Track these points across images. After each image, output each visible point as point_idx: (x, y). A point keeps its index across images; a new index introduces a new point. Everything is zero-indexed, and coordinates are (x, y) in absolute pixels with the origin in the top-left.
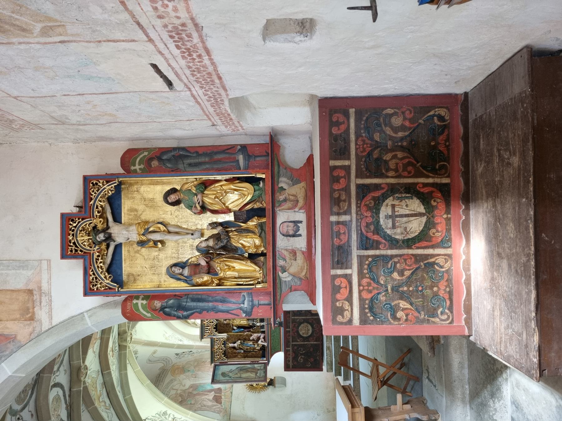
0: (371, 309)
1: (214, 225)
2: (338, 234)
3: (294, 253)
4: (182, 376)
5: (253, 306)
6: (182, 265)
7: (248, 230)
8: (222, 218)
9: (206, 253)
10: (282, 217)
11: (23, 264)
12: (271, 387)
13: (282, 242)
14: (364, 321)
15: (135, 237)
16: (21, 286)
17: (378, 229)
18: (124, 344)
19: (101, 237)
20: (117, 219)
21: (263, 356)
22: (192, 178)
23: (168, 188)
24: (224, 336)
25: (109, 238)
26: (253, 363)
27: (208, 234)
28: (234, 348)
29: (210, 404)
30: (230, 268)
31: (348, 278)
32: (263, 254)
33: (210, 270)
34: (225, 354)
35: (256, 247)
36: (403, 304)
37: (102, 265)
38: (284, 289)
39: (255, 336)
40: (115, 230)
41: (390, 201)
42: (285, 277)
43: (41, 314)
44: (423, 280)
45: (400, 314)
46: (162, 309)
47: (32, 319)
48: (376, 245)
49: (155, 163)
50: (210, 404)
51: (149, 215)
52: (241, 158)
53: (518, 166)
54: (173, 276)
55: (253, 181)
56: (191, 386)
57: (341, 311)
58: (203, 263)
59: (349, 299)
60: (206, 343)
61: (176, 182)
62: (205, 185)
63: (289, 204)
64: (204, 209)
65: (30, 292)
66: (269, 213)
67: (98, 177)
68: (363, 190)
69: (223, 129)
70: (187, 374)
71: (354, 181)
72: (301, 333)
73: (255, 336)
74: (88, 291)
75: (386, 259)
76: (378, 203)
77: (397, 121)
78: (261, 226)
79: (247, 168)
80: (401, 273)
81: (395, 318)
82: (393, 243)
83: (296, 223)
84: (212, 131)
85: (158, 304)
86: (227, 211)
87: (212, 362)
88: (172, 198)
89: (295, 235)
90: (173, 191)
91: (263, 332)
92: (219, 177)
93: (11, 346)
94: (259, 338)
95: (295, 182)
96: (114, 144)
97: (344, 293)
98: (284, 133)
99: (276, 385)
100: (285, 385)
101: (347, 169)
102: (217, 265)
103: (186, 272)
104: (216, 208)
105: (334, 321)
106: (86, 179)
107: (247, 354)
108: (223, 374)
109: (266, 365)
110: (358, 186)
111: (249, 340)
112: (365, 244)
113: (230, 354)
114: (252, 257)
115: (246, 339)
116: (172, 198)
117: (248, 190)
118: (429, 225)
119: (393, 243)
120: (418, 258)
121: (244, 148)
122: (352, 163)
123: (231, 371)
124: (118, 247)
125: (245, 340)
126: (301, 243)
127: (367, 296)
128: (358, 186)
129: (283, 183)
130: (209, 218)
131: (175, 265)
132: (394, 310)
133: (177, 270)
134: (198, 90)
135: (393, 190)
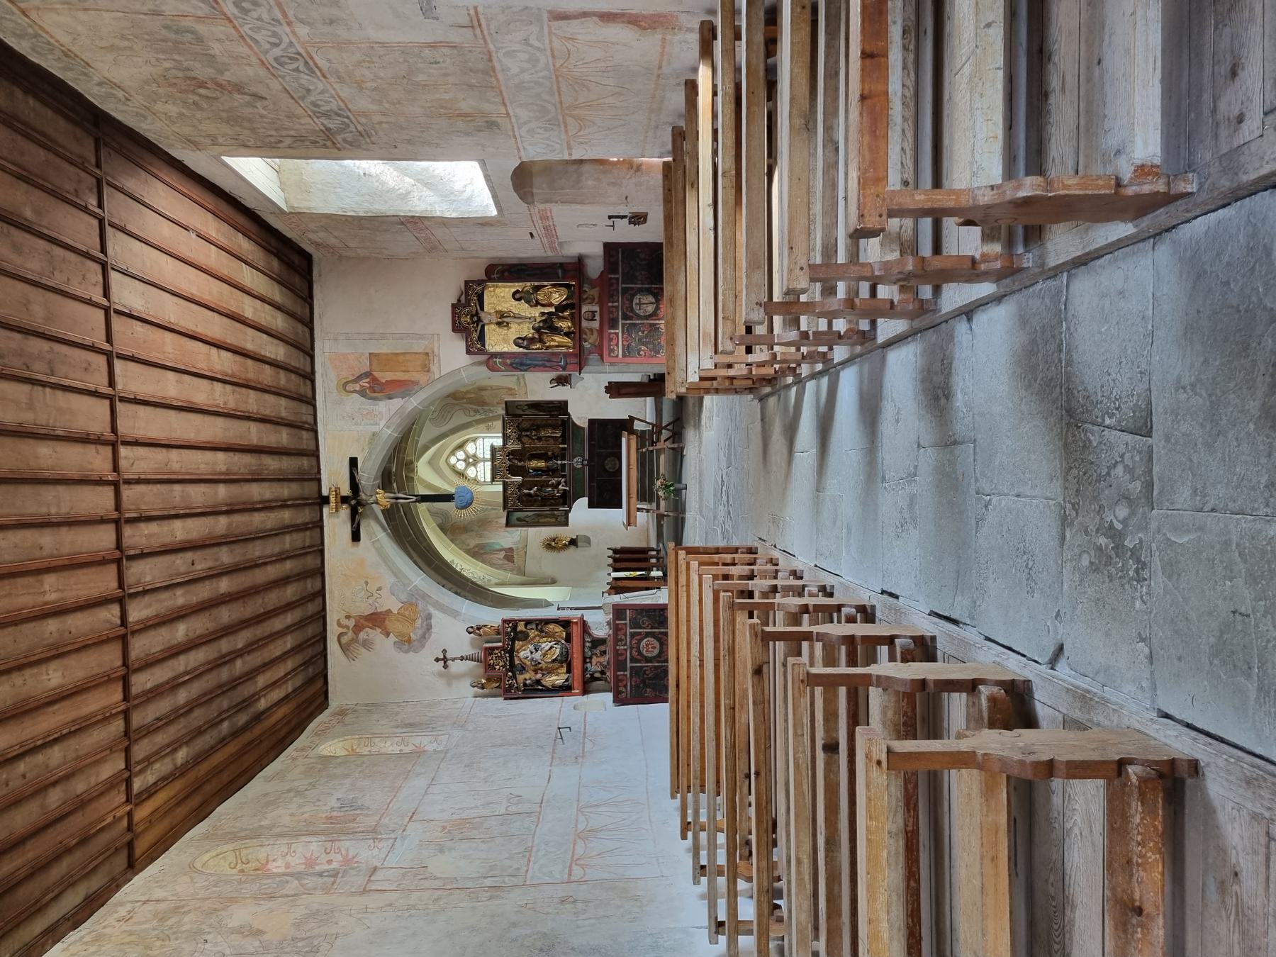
0: (628, 349)
1: (543, 314)
2: (612, 312)
3: (591, 330)
4: (464, 536)
5: (566, 364)
6: (523, 339)
7: (564, 318)
8: (547, 310)
9: (537, 330)
10: (585, 309)
11: (422, 337)
12: (572, 548)
13: (585, 324)
14: (624, 356)
15: (494, 320)
16: (421, 350)
17: (632, 310)
18: (411, 475)
19: (475, 319)
20: (482, 309)
21: (564, 504)
22: (529, 284)
23: (514, 290)
24: (519, 479)
25: (479, 320)
26: (553, 510)
27: (538, 320)
28: (529, 495)
29: (501, 562)
30: (553, 340)
31: (617, 334)
32: (573, 332)
33: (541, 341)
34: (519, 499)
35: (569, 327)
36: (643, 348)
37: (475, 336)
38: (586, 352)
39: (554, 481)
40: (482, 315)
41: (638, 296)
42: (586, 345)
43: (434, 368)
44: (653, 336)
45: (642, 353)
46: (511, 364)
47: (428, 371)
48: (630, 318)
49: (506, 274)
50: (501, 562)
51: (503, 307)
52: (560, 272)
53: (895, 283)
54: (517, 344)
55: (568, 286)
56: (476, 546)
57: (613, 351)
58: (537, 336)
59: (617, 345)
60: (499, 488)
61: (518, 286)
62: (537, 289)
63: (589, 301)
64: (538, 303)
65: (427, 354)
66: (577, 307)
67: (473, 282)
68: (625, 291)
69: (550, 254)
70: (471, 533)
71: (621, 286)
72: (607, 467)
73: (554, 481)
74: (468, 352)
75: (635, 325)
76: (633, 296)
77: (642, 256)
78: (572, 315)
79: (564, 278)
80: (643, 332)
81: (639, 354)
82: (639, 317)
83: (593, 312)
84: (545, 255)
85: (508, 361)
86: (550, 305)
87: (504, 509)
88: (518, 296)
89: (593, 319)
90: (517, 292)
91: (564, 476)
92: (546, 283)
93: (416, 387)
94: (559, 483)
95: (593, 287)
96: (479, 260)
97: (615, 341)
98: (587, 256)
99: (579, 544)
100: (589, 543)
101: (617, 279)
102: (545, 338)
103: (525, 343)
104: (544, 302)
105: (609, 355)
106: (467, 283)
107: (545, 501)
108: (519, 519)
109: (567, 513)
110: (623, 288)
111: (548, 486)
112: (625, 317)
113: (527, 501)
114: (567, 334)
115: (543, 485)
116: (518, 296)
117: (564, 291)
118: (657, 308)
119: (639, 317)
120: (652, 325)
121: (562, 265)
122: (620, 276)
123: (527, 517)
124: (483, 327)
125: (542, 486)
126: (596, 325)
127: (626, 343)
128: (623, 288)
129: (586, 287)
130: (540, 309)
131: (519, 338)
132: (639, 351)
133: (520, 341)
134: (545, 240)
135: (640, 291)
